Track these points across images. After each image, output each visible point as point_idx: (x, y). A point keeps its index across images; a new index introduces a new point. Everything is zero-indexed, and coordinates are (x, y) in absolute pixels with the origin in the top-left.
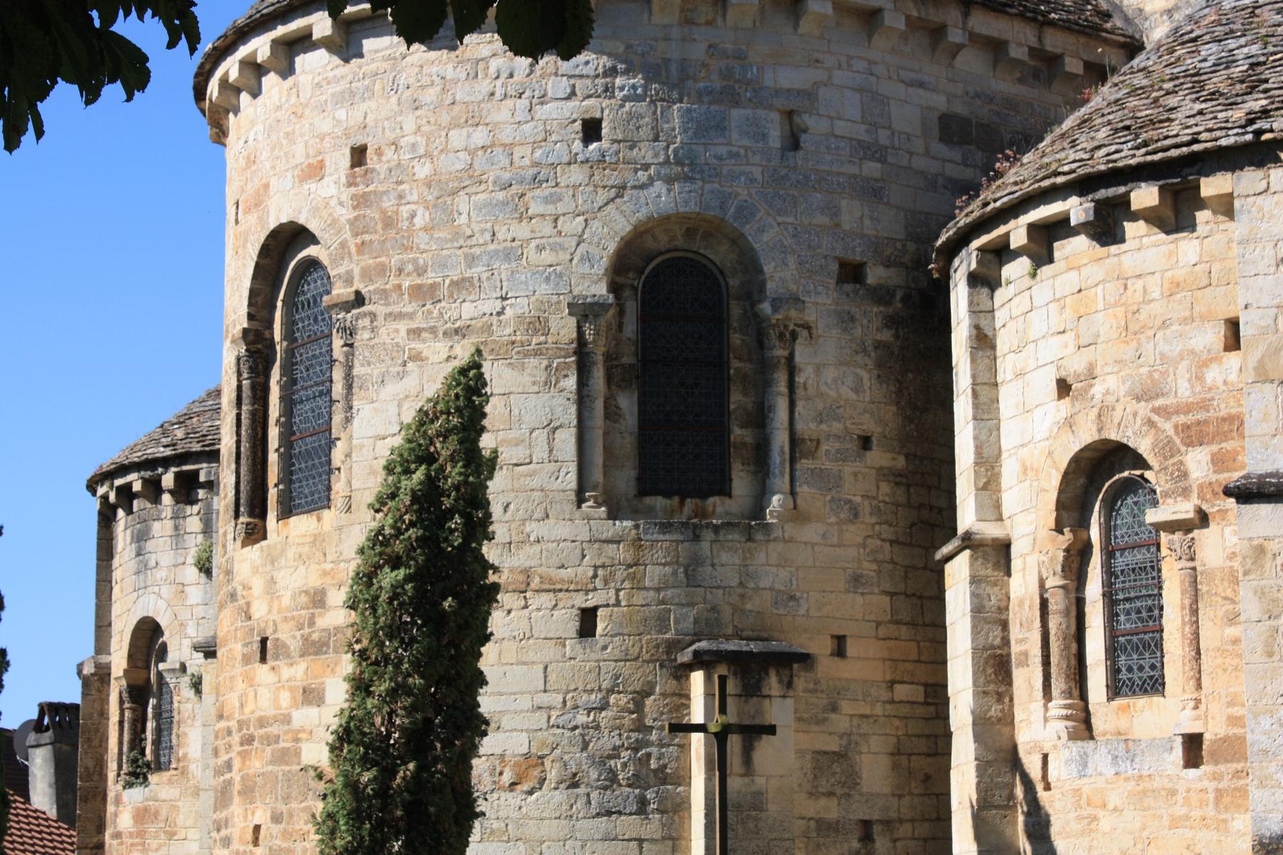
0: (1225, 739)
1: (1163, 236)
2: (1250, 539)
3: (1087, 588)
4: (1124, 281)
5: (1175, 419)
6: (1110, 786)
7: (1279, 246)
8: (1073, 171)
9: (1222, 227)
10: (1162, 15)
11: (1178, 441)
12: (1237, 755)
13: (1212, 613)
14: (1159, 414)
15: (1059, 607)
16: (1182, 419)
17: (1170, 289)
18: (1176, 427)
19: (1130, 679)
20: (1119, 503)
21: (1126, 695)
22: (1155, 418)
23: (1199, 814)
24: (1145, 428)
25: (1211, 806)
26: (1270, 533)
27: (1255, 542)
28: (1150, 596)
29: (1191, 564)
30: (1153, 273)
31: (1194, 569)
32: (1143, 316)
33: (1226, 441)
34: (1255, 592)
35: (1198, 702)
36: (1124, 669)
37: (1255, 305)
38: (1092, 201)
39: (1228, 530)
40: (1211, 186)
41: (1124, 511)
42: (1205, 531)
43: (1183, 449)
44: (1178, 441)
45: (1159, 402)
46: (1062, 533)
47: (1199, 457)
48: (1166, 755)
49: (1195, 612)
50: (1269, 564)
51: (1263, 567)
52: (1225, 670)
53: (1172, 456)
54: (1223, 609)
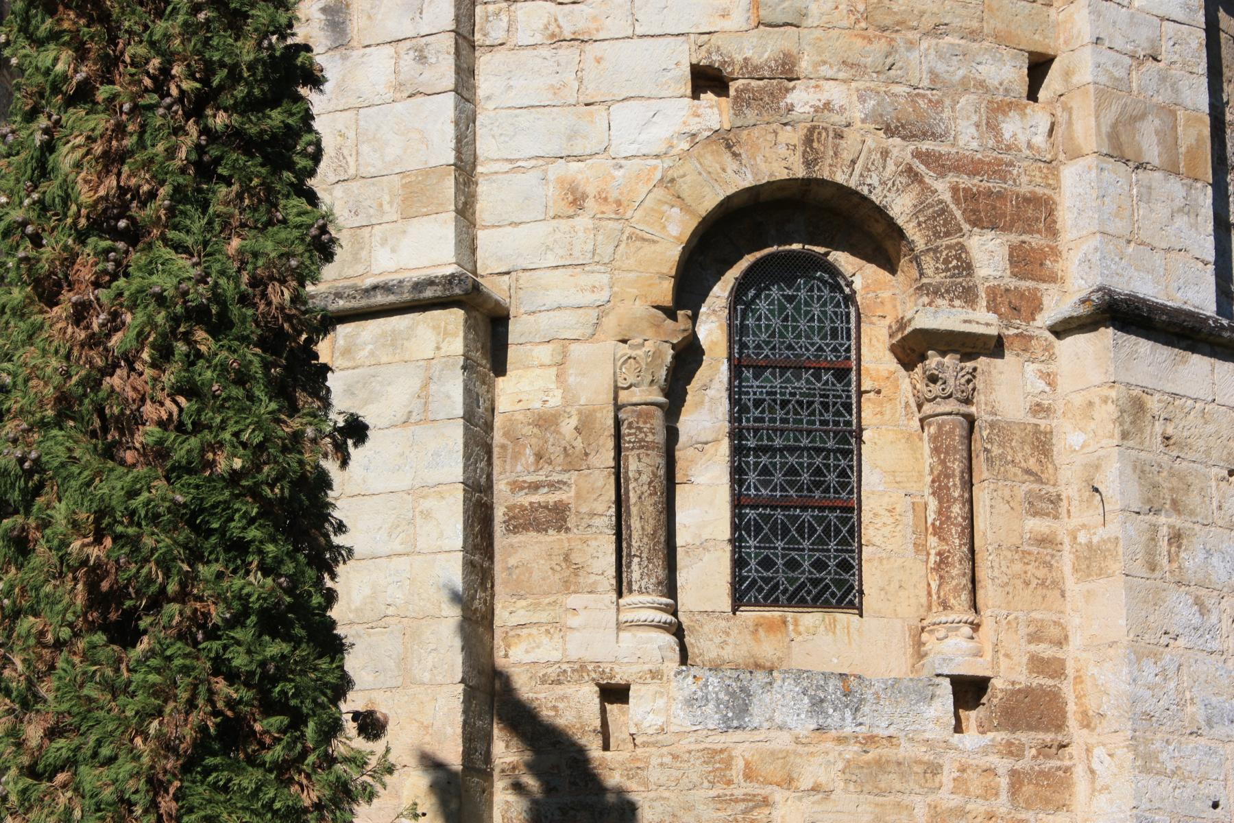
0: (1028, 692)
3: (682, 418)
5: (951, 178)
6: (800, 749)
11: (958, 214)
12: (1045, 720)
13: (1007, 492)
14: (927, 165)
16: (965, 181)
18: (955, 190)
19: (766, 580)
20: (752, 293)
21: (757, 604)
22: (921, 168)
23: (982, 809)
24: (904, 180)
25: (1004, 797)
26: (1149, 383)
27: (1137, 392)
28: (818, 451)
29: (964, 409)
31: (971, 420)
33: (1031, 232)
35: (976, 627)
36: (753, 563)
37: (1107, 44)
39: (1031, 368)
41: (762, 306)
42: (998, 361)
43: (966, 227)
44: (958, 214)
45: (926, 145)
47: (990, 246)
48: (923, 707)
50: (1149, 428)
51: (1142, 433)
52: (1027, 584)
53: (947, 234)
54: (1025, 487)
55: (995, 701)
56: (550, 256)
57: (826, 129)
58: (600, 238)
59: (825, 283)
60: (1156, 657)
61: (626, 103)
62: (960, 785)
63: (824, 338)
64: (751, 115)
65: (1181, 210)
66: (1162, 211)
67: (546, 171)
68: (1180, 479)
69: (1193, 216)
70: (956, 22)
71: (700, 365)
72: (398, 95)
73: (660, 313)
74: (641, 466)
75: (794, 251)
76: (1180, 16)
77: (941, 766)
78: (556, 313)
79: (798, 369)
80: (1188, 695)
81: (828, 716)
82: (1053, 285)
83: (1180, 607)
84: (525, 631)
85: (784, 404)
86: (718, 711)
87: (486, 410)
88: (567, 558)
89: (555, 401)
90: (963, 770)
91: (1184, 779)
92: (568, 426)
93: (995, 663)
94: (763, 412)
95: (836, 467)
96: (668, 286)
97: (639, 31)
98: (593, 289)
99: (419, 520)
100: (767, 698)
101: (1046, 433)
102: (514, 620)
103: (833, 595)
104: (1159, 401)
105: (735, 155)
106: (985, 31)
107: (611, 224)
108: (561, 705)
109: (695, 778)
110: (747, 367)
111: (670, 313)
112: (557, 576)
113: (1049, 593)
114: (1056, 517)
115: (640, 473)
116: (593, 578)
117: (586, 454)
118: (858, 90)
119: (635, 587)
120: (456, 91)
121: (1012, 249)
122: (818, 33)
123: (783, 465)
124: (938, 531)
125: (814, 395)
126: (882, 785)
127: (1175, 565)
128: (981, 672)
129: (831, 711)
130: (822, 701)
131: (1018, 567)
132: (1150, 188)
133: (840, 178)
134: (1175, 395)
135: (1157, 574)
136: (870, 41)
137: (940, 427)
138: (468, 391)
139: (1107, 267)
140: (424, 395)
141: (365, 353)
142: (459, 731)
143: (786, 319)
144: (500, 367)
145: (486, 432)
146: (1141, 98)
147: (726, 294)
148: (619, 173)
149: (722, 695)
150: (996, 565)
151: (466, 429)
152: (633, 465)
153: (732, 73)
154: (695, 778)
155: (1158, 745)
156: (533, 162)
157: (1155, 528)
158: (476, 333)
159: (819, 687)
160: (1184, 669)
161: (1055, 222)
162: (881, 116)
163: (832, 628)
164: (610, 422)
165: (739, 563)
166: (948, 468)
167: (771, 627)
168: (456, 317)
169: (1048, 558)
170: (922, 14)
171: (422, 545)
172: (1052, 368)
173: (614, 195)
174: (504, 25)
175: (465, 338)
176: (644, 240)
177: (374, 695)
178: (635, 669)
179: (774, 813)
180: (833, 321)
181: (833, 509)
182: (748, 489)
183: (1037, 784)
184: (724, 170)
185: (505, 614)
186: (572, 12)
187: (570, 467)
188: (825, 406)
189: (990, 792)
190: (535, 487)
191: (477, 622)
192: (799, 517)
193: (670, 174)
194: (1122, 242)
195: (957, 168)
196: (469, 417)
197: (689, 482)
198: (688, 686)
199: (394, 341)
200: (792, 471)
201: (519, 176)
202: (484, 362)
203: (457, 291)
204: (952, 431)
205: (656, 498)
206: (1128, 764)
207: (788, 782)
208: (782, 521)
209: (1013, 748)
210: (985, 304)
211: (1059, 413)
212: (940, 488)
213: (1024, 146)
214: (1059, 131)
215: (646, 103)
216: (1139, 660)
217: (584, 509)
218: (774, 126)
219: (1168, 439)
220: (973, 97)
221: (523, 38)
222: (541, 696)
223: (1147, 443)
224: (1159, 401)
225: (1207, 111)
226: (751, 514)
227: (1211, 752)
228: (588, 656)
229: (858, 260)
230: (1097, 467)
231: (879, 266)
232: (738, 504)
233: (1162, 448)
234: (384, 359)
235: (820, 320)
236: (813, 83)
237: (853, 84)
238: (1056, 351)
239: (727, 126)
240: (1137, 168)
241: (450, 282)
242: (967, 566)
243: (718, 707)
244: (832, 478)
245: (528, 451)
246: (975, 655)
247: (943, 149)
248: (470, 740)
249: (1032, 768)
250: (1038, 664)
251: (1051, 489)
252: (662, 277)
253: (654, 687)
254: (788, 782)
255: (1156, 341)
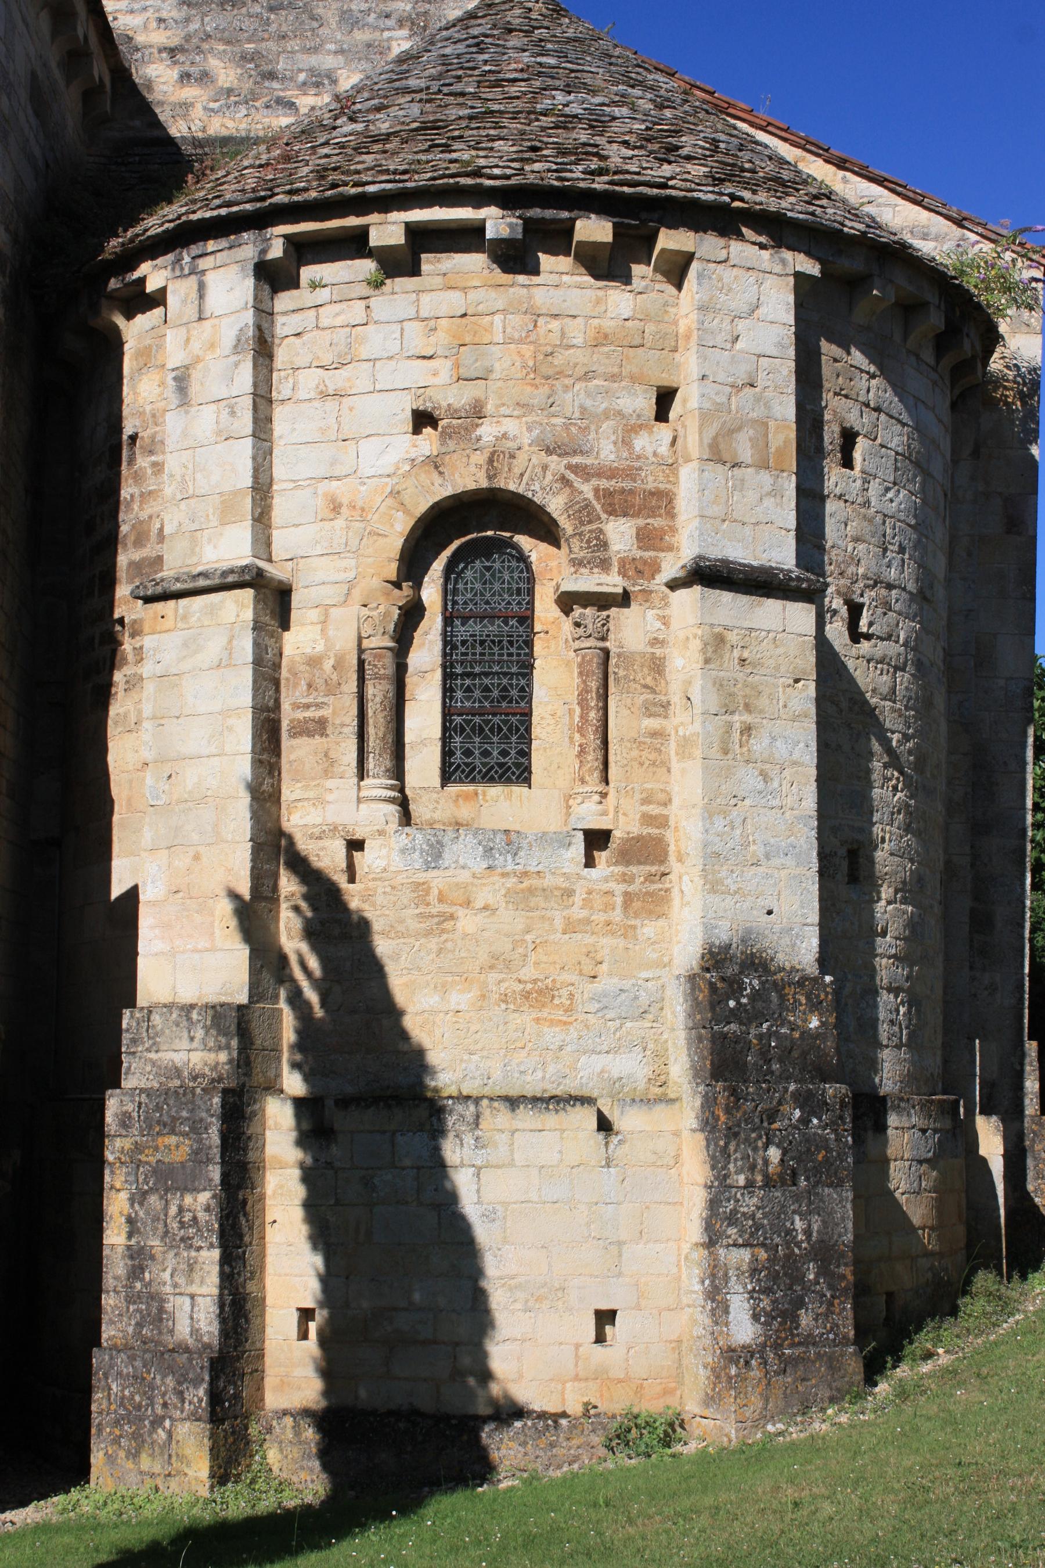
0: (639, 839)
1: (589, 279)
2: (712, 625)
3: (410, 655)
4: (535, 317)
5: (594, 482)
7: (735, 323)
8: (508, 177)
9: (658, 286)
10: (160, 51)
11: (598, 507)
12: (651, 857)
13: (629, 701)
14: (576, 474)
15: (387, 672)
16: (604, 484)
17: (596, 339)
18: (596, 490)
19: (467, 765)
20: (462, 565)
21: (461, 781)
22: (571, 476)
23: (602, 919)
24: (558, 485)
26: (729, 623)
27: (717, 630)
28: (505, 674)
29: (601, 644)
30: (575, 317)
31: (606, 652)
32: (558, 360)
33: (654, 516)
34: (715, 683)
35: (604, 795)
36: (458, 753)
37: (711, 379)
38: (519, 217)
39: (651, 614)
40: (669, 240)
41: (469, 574)
42: (626, 610)
43: (604, 516)
44: (598, 507)
45: (576, 460)
46: (400, 588)
47: (622, 528)
48: (563, 851)
49: (604, 696)
50: (728, 655)
52: (641, 764)
53: (590, 522)
54: (642, 697)
55: (614, 846)
56: (318, 547)
57: (503, 452)
58: (350, 534)
59: (513, 556)
60: (725, 814)
61: (369, 439)
62: (587, 903)
63: (511, 595)
64: (451, 444)
65: (769, 494)
66: (752, 496)
67: (316, 488)
68: (753, 688)
69: (778, 497)
70: (601, 370)
71: (423, 617)
72: (219, 439)
73: (389, 585)
74: (376, 691)
75: (487, 537)
76: (774, 353)
77: (574, 891)
78: (322, 587)
79: (492, 618)
80: (751, 838)
81: (495, 859)
82: (670, 553)
83: (748, 779)
84: (300, 804)
85: (482, 643)
86: (422, 856)
87: (274, 655)
88: (326, 755)
89: (320, 648)
90: (589, 893)
91: (744, 896)
92: (328, 665)
93: (616, 819)
94: (467, 648)
95: (517, 685)
96: (395, 565)
97: (378, 387)
98: (345, 570)
99: (226, 733)
100: (455, 847)
101: (660, 659)
102: (293, 797)
103: (513, 773)
104: (737, 635)
105: (441, 473)
106: (624, 374)
107: (358, 524)
108: (322, 853)
109: (405, 901)
110: (457, 618)
111: (397, 585)
112: (320, 767)
113: (658, 770)
114: (666, 717)
115: (375, 696)
116: (343, 768)
117: (339, 684)
118: (527, 423)
119: (371, 774)
120: (254, 435)
121: (639, 530)
122: (500, 384)
123: (481, 685)
124: (581, 730)
125: (503, 636)
126: (532, 904)
127: (746, 749)
128: (604, 827)
129: (497, 856)
130: (491, 849)
131: (635, 753)
132: (743, 480)
133: (512, 487)
134: (751, 629)
135: (730, 756)
136: (537, 387)
137: (583, 657)
138: (256, 644)
139: (704, 540)
140: (229, 648)
141: (194, 619)
142: (249, 873)
143: (485, 583)
144: (285, 625)
145: (274, 670)
146: (739, 415)
147: (441, 568)
148: (363, 488)
149: (424, 846)
150: (618, 752)
151: (255, 671)
152: (370, 690)
153: (440, 415)
154: (405, 901)
155: (723, 874)
156: (308, 482)
157: (730, 725)
158: (265, 604)
159: (489, 840)
160: (749, 821)
161: (674, 508)
162: (543, 440)
163: (509, 797)
164: (355, 662)
165: (447, 753)
166: (587, 686)
167: (467, 797)
168: (248, 594)
169: (659, 746)
170: (576, 365)
171: (228, 749)
172: (667, 612)
173: (360, 504)
174: (291, 385)
175: (255, 608)
176: (379, 535)
177: (199, 848)
178: (368, 829)
179: (458, 924)
180: (518, 583)
181: (514, 714)
182: (456, 702)
183: (644, 901)
184: (433, 484)
185: (289, 792)
186: (334, 375)
187: (329, 693)
188: (511, 643)
189: (609, 907)
190: (307, 706)
191: (265, 799)
192: (491, 720)
193: (397, 488)
194: (718, 522)
195: (599, 474)
196: (258, 662)
197: (414, 699)
198: (403, 840)
199: (212, 611)
200: (487, 689)
201: (299, 491)
202: (273, 623)
203: (247, 577)
204: (591, 660)
205: (386, 713)
206: (700, 888)
207: (468, 903)
208: (480, 725)
209: (626, 878)
210: (616, 570)
211: (671, 644)
212: (582, 699)
213: (650, 455)
214: (680, 442)
215: (381, 438)
216: (710, 817)
217: (337, 722)
218: (468, 451)
219: (744, 660)
220: (612, 422)
221: (302, 395)
222: (310, 847)
223: (726, 665)
224: (737, 635)
225: (794, 420)
226: (458, 719)
227: (768, 876)
228: (338, 820)
229: (534, 540)
230: (690, 683)
231: (550, 544)
232: (447, 713)
233: (738, 667)
234: (206, 623)
235: (509, 583)
236: (495, 419)
237: (524, 419)
238: (670, 600)
239: (435, 453)
240: (733, 467)
241: (243, 571)
242: (600, 755)
243: (421, 854)
244: (514, 693)
245: (303, 682)
246: (601, 815)
247: (589, 461)
248: (258, 879)
249: (640, 890)
250: (648, 819)
251: (663, 698)
252: (390, 560)
253: (380, 841)
254: (468, 903)
255: (737, 592)
